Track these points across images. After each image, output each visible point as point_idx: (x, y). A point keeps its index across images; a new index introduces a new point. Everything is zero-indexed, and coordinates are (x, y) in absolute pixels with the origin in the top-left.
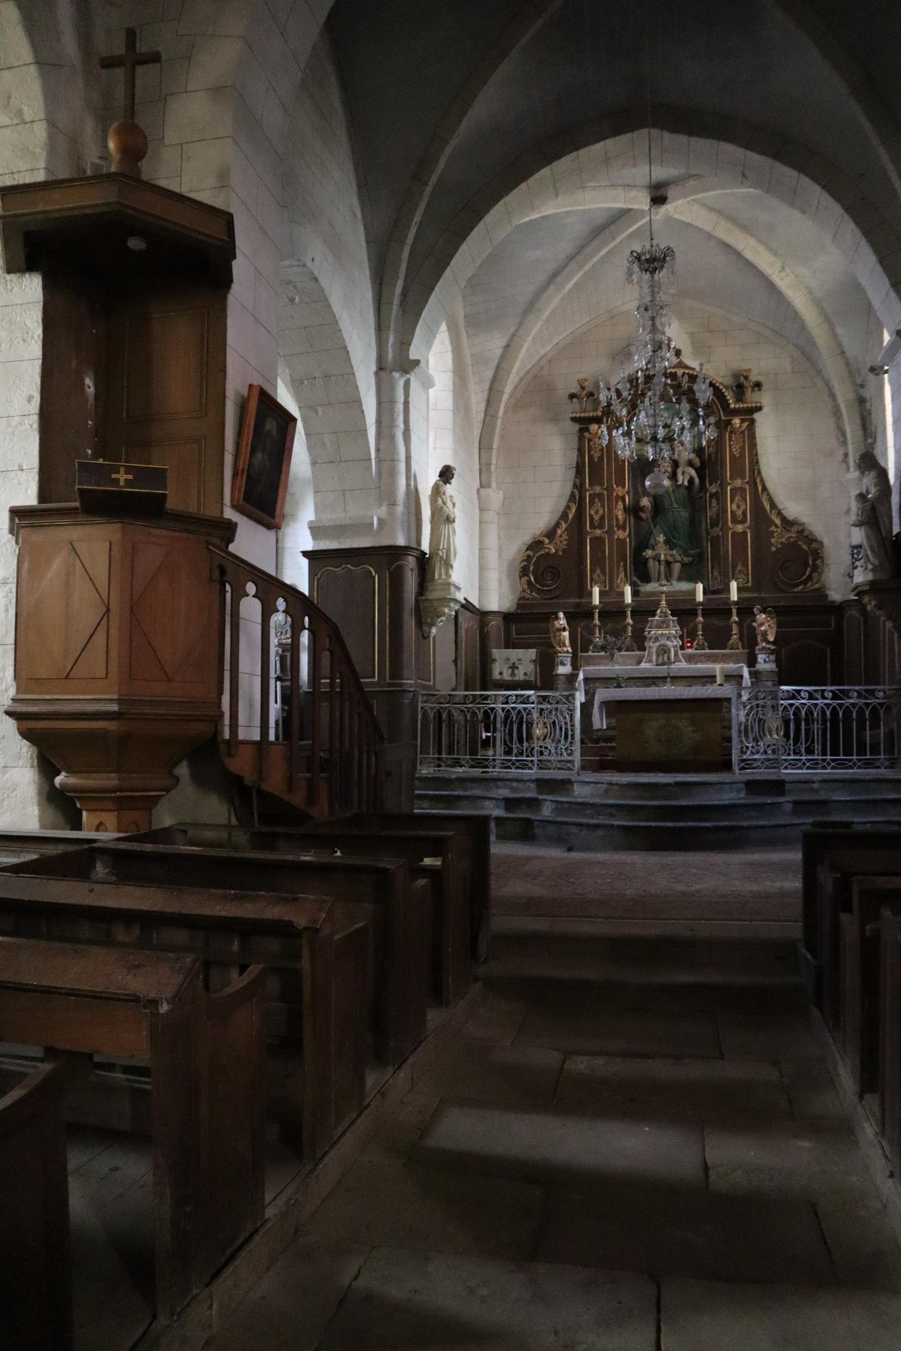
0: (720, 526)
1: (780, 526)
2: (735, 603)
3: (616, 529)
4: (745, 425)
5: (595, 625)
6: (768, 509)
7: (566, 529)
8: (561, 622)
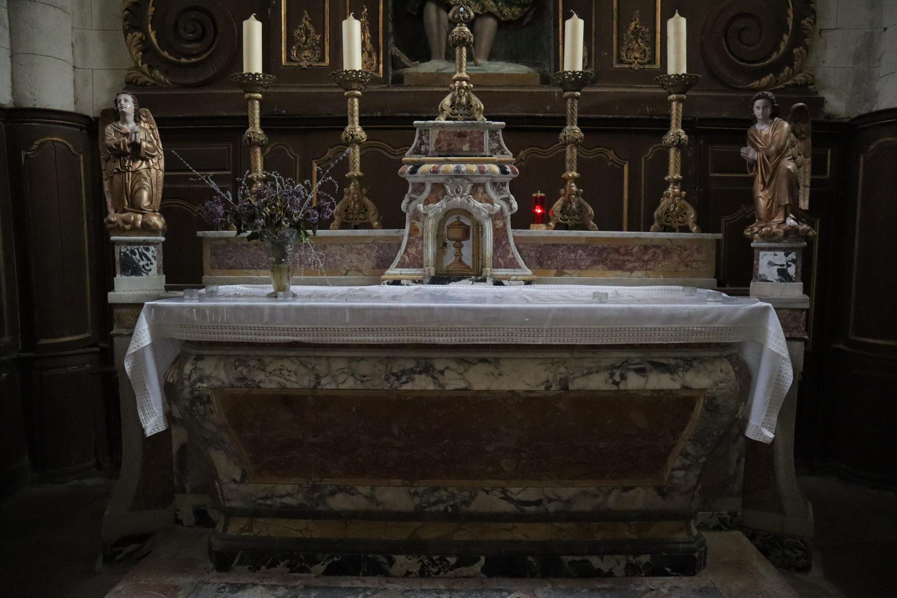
5: (252, 144)
8: (130, 126)
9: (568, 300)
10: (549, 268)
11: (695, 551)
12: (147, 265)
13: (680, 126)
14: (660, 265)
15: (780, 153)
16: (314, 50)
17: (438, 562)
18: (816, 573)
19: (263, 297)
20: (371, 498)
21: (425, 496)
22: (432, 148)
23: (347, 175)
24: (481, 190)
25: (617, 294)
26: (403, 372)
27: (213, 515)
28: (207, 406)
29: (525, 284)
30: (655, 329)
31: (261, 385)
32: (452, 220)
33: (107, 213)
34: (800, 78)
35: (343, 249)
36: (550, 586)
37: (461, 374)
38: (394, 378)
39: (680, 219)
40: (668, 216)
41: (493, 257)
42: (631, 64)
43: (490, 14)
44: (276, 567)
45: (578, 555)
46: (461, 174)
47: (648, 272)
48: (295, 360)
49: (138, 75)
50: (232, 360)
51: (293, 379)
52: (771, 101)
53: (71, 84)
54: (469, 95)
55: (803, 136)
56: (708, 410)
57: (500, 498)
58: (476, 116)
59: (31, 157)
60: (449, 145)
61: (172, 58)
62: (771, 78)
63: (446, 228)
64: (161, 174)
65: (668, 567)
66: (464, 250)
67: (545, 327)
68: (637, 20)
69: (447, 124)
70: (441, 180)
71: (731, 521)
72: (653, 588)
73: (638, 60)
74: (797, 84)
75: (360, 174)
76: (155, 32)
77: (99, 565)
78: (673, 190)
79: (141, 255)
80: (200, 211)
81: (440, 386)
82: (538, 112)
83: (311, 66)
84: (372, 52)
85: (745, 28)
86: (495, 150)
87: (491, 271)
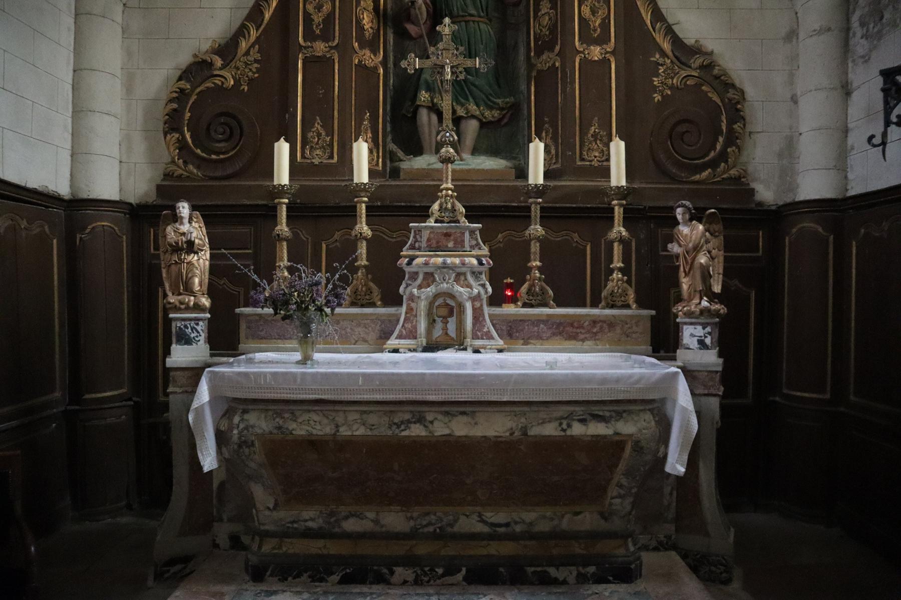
0: (558, 48)
1: (670, 54)
2: (621, 193)
5: (279, 238)
6: (648, 22)
7: (258, 38)
8: (185, 227)
10: (517, 338)
11: (631, 563)
12: (197, 337)
13: (621, 225)
15: (697, 249)
16: (324, 149)
18: (736, 585)
19: (292, 363)
20: (376, 522)
21: (419, 520)
22: (424, 245)
23: (356, 264)
24: (462, 278)
25: (570, 361)
26: (402, 422)
27: (246, 540)
28: (252, 448)
30: (592, 389)
31: (294, 432)
32: (440, 301)
34: (733, 173)
36: (516, 591)
37: (446, 424)
38: (395, 426)
39: (623, 299)
42: (591, 161)
43: (473, 117)
45: (538, 566)
48: (320, 412)
49: (174, 168)
50: (270, 413)
51: (318, 427)
53: (117, 176)
54: (453, 201)
55: (717, 234)
56: (635, 451)
57: (478, 521)
59: (85, 239)
60: (438, 242)
62: (710, 173)
64: (207, 263)
65: (610, 576)
66: (449, 326)
67: (509, 388)
68: (596, 124)
71: (667, 543)
72: (597, 591)
73: (598, 158)
74: (732, 178)
75: (367, 263)
76: (190, 133)
77: (150, 582)
78: (616, 275)
79: (192, 328)
80: (224, 284)
81: (430, 432)
83: (321, 162)
85: (687, 132)
86: (473, 246)
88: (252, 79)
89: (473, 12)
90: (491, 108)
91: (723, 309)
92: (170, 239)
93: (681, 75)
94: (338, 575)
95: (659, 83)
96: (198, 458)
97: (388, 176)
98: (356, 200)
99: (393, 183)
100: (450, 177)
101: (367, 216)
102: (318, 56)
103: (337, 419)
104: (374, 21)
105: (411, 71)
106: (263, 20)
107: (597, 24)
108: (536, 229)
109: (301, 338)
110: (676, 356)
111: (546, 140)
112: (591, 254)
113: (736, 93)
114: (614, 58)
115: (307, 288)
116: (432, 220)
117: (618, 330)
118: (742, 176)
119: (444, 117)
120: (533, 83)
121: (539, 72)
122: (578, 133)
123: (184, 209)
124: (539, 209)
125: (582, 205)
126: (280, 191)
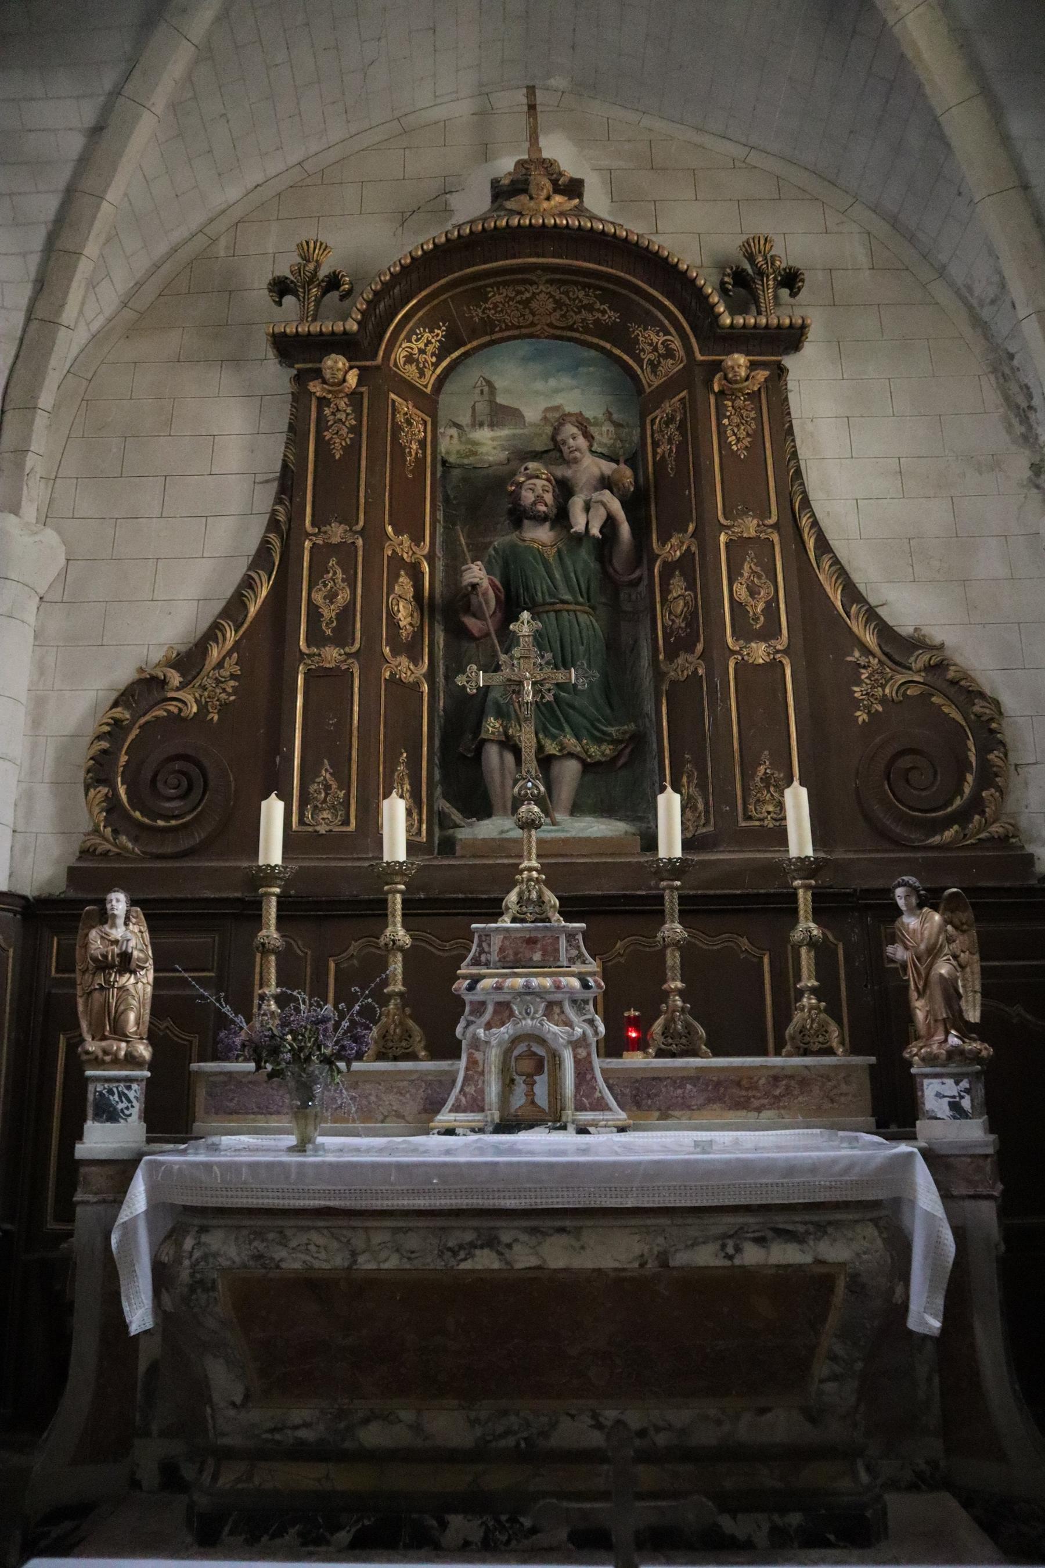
0: (700, 647)
1: (876, 650)
2: (807, 868)
3: (387, 650)
4: (762, 375)
6: (838, 604)
7: (237, 643)
8: (118, 932)
9: (669, 1151)
10: (649, 1108)
12: (127, 1108)
14: (795, 1101)
15: (933, 952)
16: (336, 810)
17: (507, 1525)
21: (490, 1424)
22: (494, 957)
23: (385, 991)
24: (557, 1010)
26: (461, 1247)
27: (188, 1472)
28: (211, 1294)
29: (618, 1132)
31: (284, 1265)
32: (521, 1049)
33: (83, 1040)
35: (380, 1087)
38: (450, 1254)
39: (821, 1039)
40: (804, 1035)
41: (575, 1096)
42: (762, 820)
43: (571, 755)
44: (283, 1536)
46: (531, 990)
47: (782, 1112)
48: (325, 1232)
50: (245, 1232)
51: (323, 1255)
52: (915, 889)
53: (8, 855)
55: (965, 927)
57: (591, 1426)
58: (550, 914)
60: (516, 954)
61: (146, 820)
62: (957, 832)
63: (513, 1059)
64: (149, 989)
68: (767, 763)
69: (513, 928)
70: (508, 998)
74: (993, 837)
75: (403, 989)
76: (125, 787)
78: (808, 1001)
79: (121, 1095)
80: (167, 1027)
81: (507, 1263)
82: (640, 889)
83: (331, 831)
84: (413, 808)
85: (912, 768)
86: (573, 958)
87: (573, 1115)
88: (226, 704)
89: (568, 597)
90: (599, 741)
91: (986, 1048)
92: (95, 949)
93: (896, 682)
94: (348, 1532)
95: (862, 695)
96: (121, 1311)
97: (436, 851)
98: (386, 888)
99: (446, 862)
100: (534, 851)
101: (403, 915)
102: (329, 668)
103: (353, 1241)
104: (415, 614)
105: (471, 691)
106: (246, 616)
107: (759, 610)
108: (674, 929)
109: (298, 1108)
110: (915, 1133)
111: (688, 787)
112: (771, 971)
113: (988, 705)
114: (788, 660)
115: (309, 1027)
116: (507, 918)
117: (816, 1090)
118: (1010, 835)
119: (523, 758)
120: (664, 701)
121: (673, 683)
122: (738, 777)
123: (119, 902)
124: (676, 897)
125: (750, 891)
126: (268, 875)
